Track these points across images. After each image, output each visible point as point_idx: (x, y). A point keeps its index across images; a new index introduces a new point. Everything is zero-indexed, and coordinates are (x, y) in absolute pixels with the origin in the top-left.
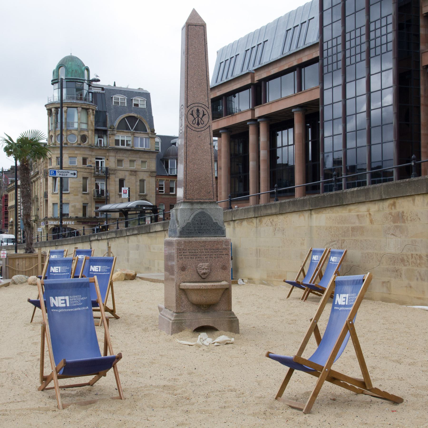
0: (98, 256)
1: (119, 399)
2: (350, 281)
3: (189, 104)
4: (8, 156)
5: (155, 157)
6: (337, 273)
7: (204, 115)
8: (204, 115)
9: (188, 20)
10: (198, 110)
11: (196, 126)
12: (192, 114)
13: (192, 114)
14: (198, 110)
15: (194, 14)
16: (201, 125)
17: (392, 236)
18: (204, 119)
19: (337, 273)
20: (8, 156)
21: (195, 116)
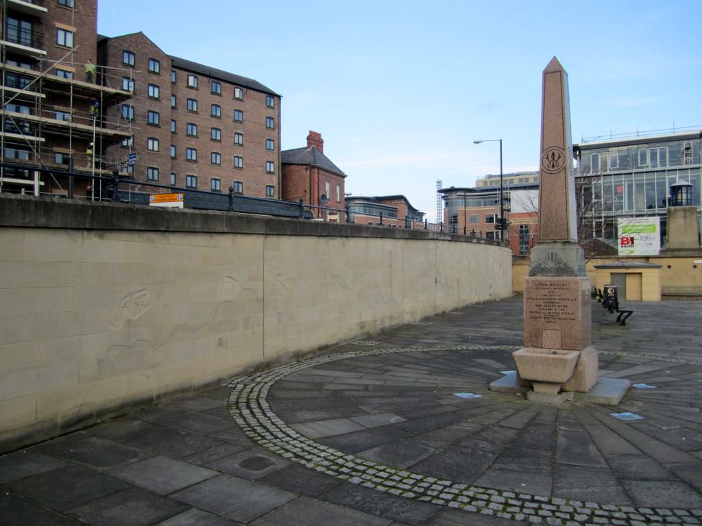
0: (680, 284)
1: (641, 277)
2: (109, 128)
3: (545, 149)
4: (311, 132)
5: (619, 254)
6: (131, 193)
7: (559, 157)
8: (559, 157)
9: (546, 68)
10: (553, 154)
11: (551, 169)
12: (547, 158)
13: (547, 158)
14: (553, 154)
15: (554, 61)
16: (556, 168)
17: (230, 280)
18: (559, 161)
19: (131, 193)
20: (311, 132)
21: (550, 159)
